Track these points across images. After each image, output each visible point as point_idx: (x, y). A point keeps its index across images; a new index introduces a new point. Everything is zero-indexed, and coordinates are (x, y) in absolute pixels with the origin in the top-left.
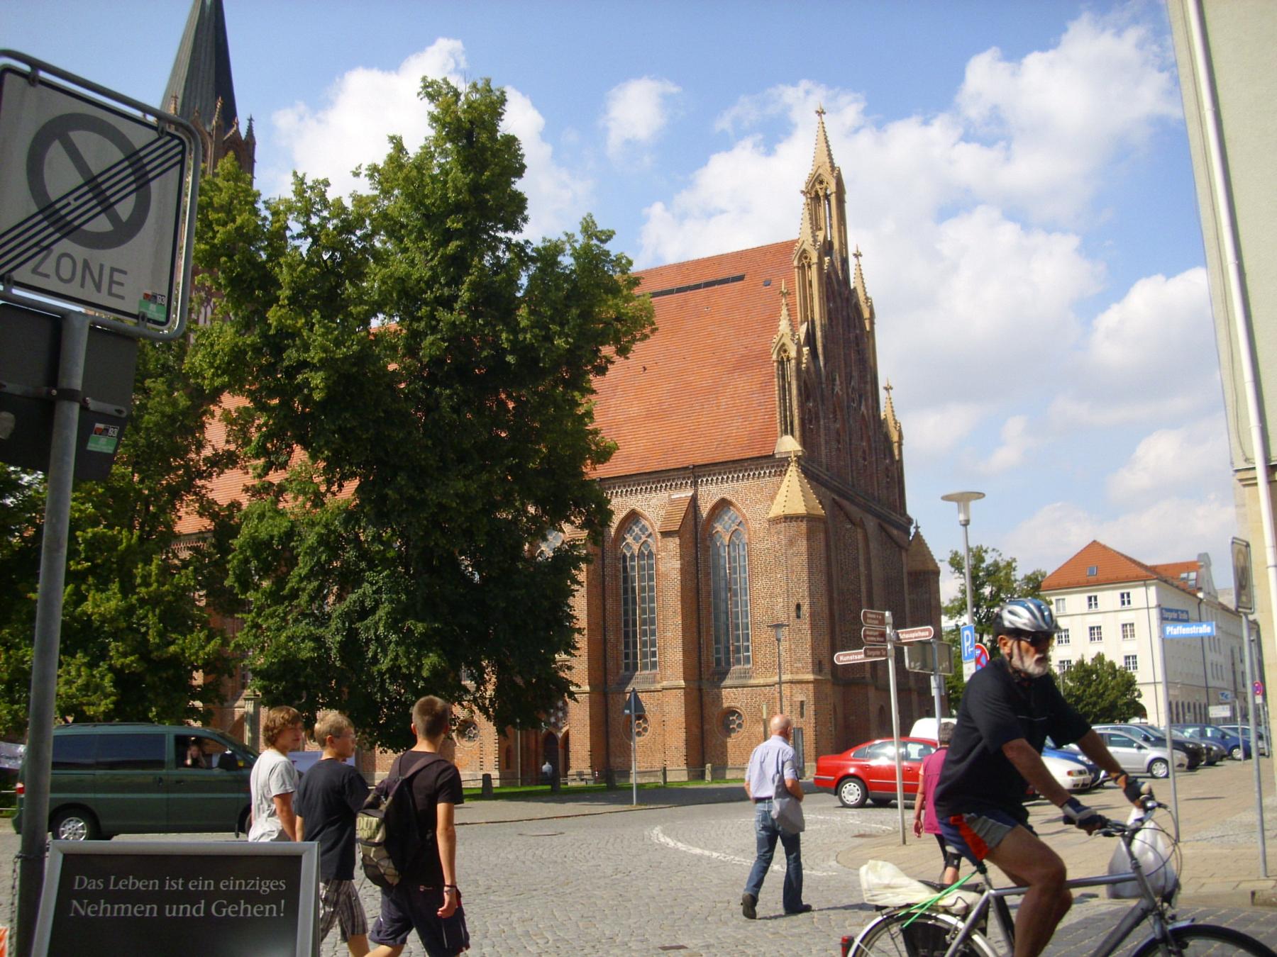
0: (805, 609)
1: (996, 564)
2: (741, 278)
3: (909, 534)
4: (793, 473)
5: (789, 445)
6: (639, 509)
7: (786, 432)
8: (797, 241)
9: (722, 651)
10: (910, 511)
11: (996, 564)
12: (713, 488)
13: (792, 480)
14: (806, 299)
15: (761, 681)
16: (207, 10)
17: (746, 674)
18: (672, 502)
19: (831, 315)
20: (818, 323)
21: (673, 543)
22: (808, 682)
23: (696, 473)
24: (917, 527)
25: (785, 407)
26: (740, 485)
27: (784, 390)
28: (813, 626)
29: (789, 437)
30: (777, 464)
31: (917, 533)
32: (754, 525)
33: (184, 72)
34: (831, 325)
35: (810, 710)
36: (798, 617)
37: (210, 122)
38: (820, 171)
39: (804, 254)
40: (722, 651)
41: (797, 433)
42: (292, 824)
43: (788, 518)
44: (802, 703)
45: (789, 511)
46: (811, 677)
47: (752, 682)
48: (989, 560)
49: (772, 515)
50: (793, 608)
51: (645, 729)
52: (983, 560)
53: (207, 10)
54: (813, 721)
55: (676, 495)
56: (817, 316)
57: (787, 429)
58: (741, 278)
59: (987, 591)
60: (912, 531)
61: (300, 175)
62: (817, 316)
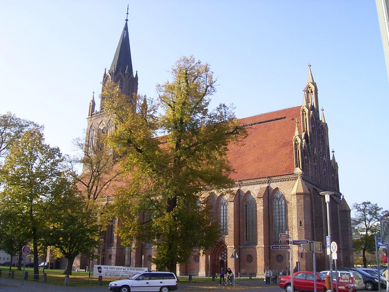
24: (343, 196)
29: (298, 168)
31: (343, 198)
41: (301, 167)
60: (342, 197)
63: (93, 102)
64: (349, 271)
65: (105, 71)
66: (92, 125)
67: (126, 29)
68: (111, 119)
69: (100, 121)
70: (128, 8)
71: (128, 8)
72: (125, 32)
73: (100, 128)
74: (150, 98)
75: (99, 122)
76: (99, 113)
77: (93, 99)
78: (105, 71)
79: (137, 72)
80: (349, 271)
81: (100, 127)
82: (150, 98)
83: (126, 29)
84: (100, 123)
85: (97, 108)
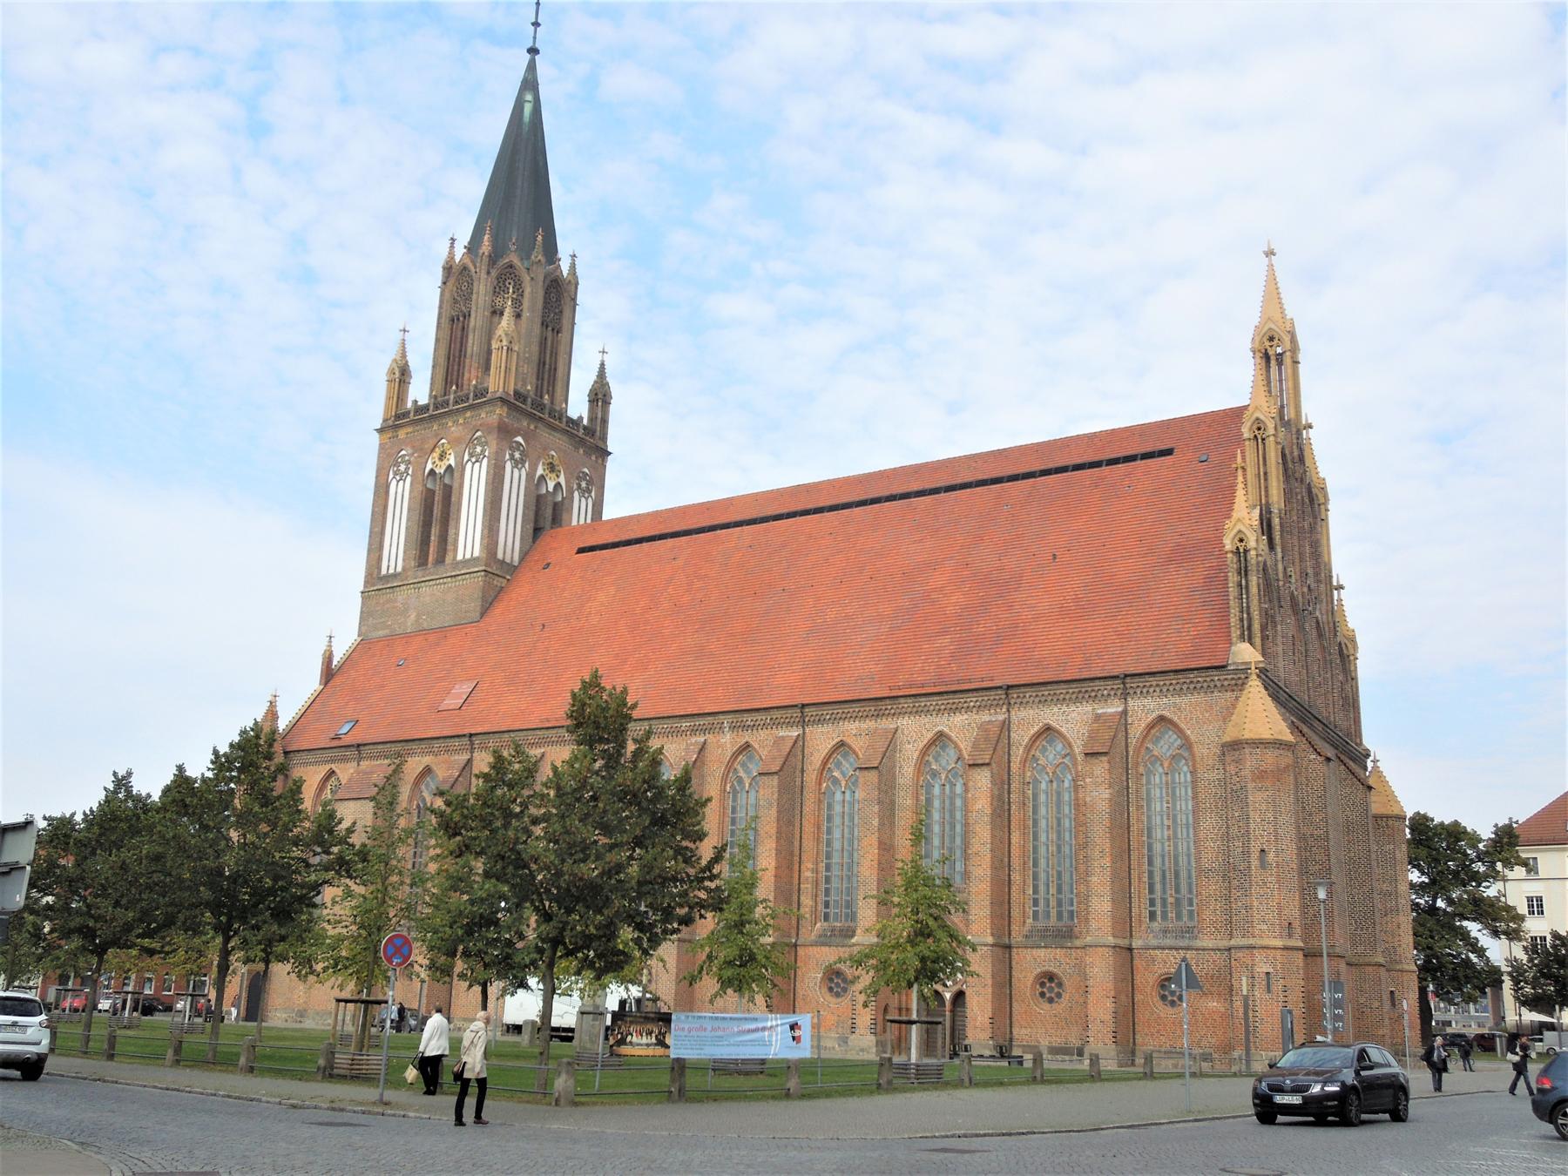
2: (1169, 452)
3: (1365, 769)
4: (1255, 687)
6: (1054, 725)
8: (1246, 408)
9: (1158, 902)
12: (1149, 703)
18: (1098, 717)
19: (1288, 494)
21: (1100, 768)
23: (1126, 682)
26: (1184, 701)
31: (1375, 768)
39: (1259, 426)
40: (1158, 902)
41: (1258, 641)
46: (1279, 943)
47: (1199, 943)
49: (1227, 738)
50: (1255, 855)
51: (1059, 995)
53: (526, 128)
55: (985, 717)
58: (1169, 452)
60: (1370, 765)
61: (121, 773)
64: (577, 406)
72: (529, 97)
73: (432, 471)
76: (425, 408)
77: (404, 355)
80: (577, 406)
81: (429, 466)
85: (420, 391)
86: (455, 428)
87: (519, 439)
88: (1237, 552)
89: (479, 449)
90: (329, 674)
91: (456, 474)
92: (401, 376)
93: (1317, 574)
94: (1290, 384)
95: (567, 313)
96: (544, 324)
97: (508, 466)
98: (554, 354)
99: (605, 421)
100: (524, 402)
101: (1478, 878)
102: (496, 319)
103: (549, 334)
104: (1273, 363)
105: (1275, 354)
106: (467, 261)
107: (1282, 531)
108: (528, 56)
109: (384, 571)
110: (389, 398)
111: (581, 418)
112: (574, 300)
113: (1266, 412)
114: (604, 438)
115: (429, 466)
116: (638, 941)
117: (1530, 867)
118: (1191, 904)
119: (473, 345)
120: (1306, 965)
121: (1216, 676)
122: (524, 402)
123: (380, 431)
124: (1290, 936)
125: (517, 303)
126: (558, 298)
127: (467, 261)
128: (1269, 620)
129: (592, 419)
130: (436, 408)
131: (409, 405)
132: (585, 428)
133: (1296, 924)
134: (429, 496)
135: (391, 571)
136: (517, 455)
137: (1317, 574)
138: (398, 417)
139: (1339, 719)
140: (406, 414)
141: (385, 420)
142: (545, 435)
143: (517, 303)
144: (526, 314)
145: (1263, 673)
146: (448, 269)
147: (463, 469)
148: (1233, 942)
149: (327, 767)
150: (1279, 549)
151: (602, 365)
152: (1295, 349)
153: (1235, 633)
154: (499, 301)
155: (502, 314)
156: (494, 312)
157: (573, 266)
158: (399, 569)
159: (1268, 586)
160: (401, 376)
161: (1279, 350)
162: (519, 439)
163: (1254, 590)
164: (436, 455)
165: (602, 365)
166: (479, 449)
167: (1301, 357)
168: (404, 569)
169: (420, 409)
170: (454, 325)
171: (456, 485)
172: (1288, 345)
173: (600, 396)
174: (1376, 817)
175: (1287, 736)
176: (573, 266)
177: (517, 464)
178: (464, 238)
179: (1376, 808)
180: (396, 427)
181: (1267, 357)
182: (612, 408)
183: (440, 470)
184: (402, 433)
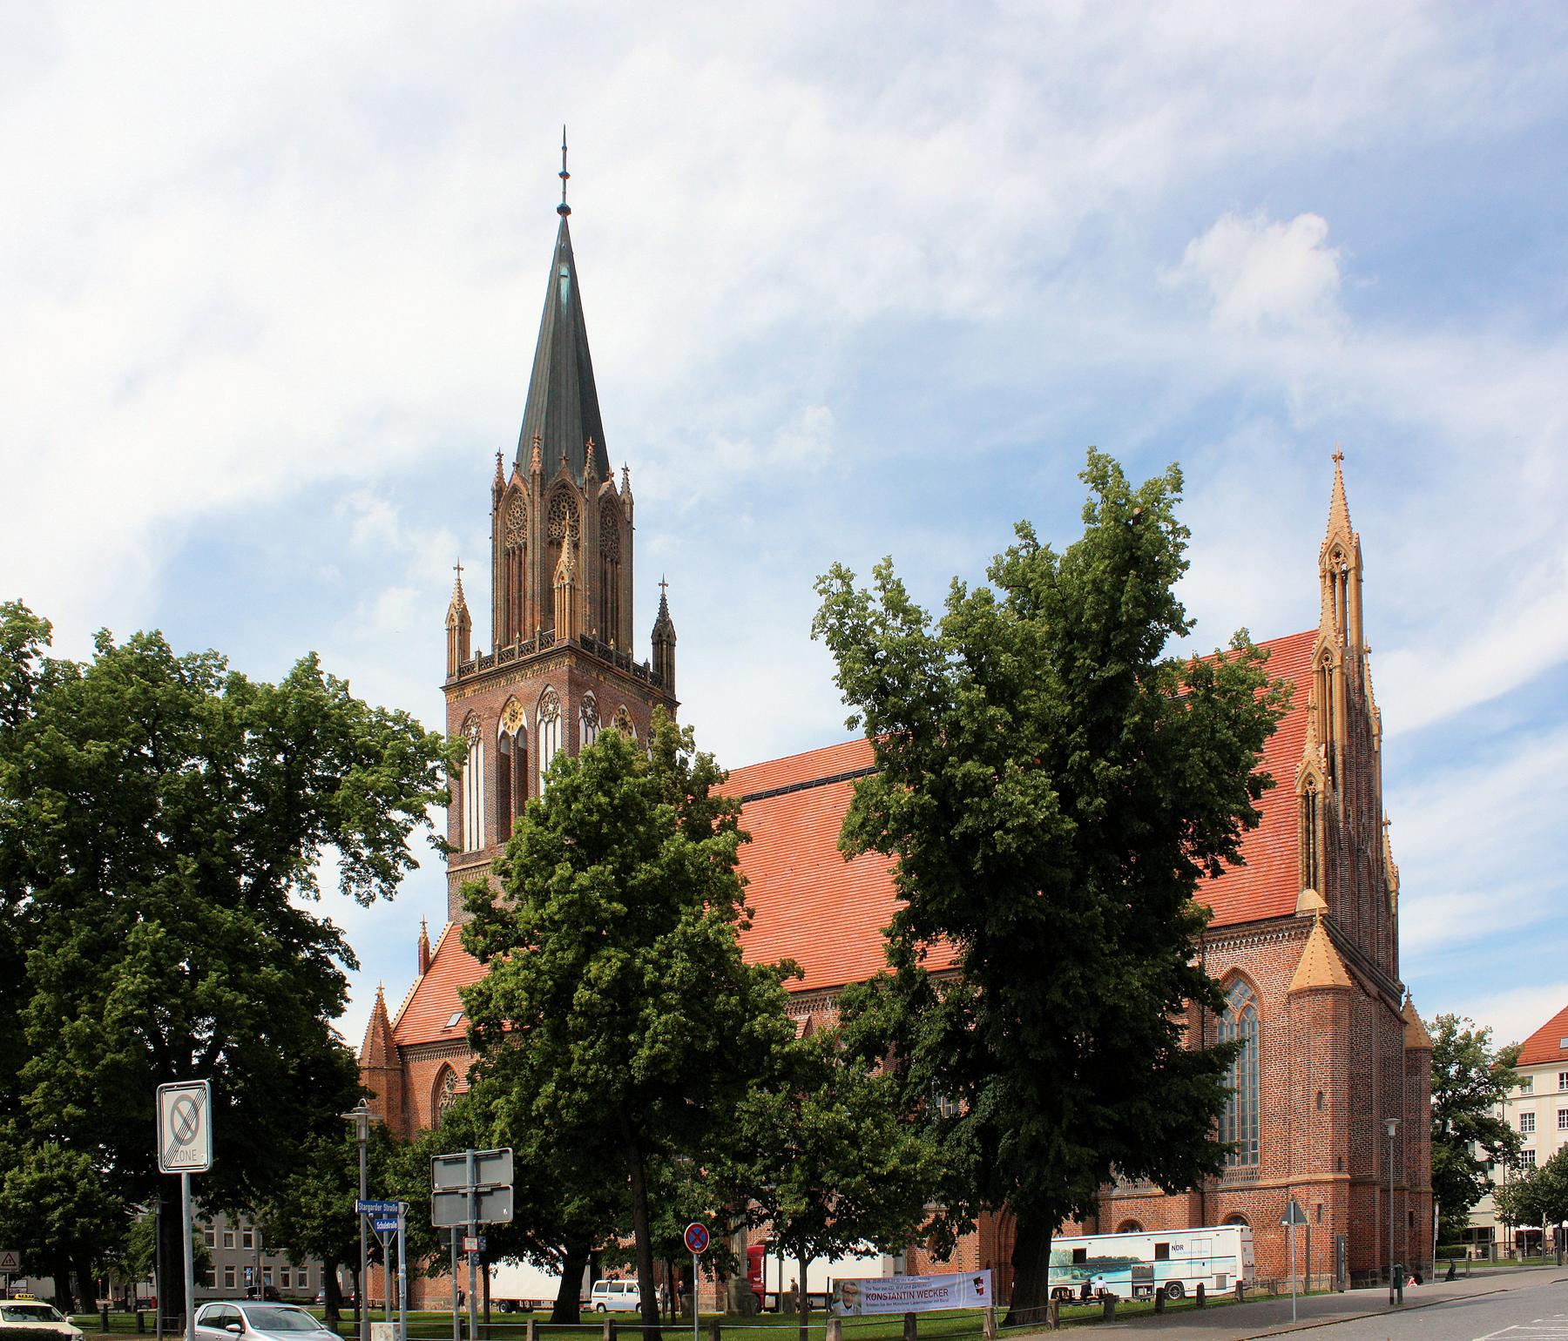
0: (1327, 1097)
1: (1467, 1036)
4: (1318, 935)
5: (1312, 901)
7: (1308, 885)
10: (1403, 977)
11: (1467, 1036)
13: (1318, 942)
14: (1327, 713)
15: (1271, 1182)
16: (564, 311)
17: (1253, 1175)
20: (1338, 745)
22: (1327, 1183)
24: (1408, 996)
25: (1310, 855)
27: (1309, 833)
28: (1334, 1118)
29: (1312, 891)
30: (1298, 926)
31: (1408, 1002)
32: (1268, 1000)
33: (543, 401)
34: (1350, 746)
35: (1327, 1214)
36: (1319, 1107)
37: (581, 474)
38: (1337, 540)
41: (1321, 886)
42: (1338, 1272)
43: (1315, 991)
44: (1320, 1206)
45: (1313, 983)
46: (1330, 1177)
47: (1261, 1183)
48: (1460, 1030)
49: (1293, 987)
50: (1314, 1097)
52: (1453, 1033)
53: (564, 311)
54: (1330, 1226)
56: (1337, 735)
57: (1311, 883)
59: (1453, 1070)
60: (1404, 1000)
62: (1337, 735)
63: (464, 618)
64: (643, 652)
65: (500, 464)
66: (466, 719)
67: (564, 254)
68: (550, 689)
69: (502, 700)
70: (565, 148)
71: (565, 148)
72: (564, 271)
73: (504, 733)
74: (626, 470)
75: (498, 705)
76: (490, 660)
77: (461, 598)
78: (500, 464)
79: (663, 584)
80: (643, 652)
81: (501, 728)
82: (626, 470)
83: (564, 254)
84: (503, 710)
85: (482, 641)
86: (526, 684)
87: (590, 693)
88: (1306, 797)
89: (551, 707)
90: (427, 964)
91: (531, 737)
92: (461, 626)
93: (1370, 810)
94: (1354, 604)
95: (623, 540)
96: (604, 556)
97: (582, 724)
98: (615, 590)
99: (671, 667)
100: (591, 650)
101: (1482, 1102)
102: (553, 551)
103: (609, 565)
104: (1338, 581)
105: (1024, 531)
106: (517, 481)
107: (1344, 769)
108: (559, 218)
109: (467, 849)
110: (451, 651)
111: (647, 664)
112: (630, 523)
113: (1331, 640)
114: (671, 686)
115: (501, 728)
116: (503, 1134)
117: (1525, 1083)
118: (1254, 1148)
119: (532, 583)
120: (1351, 1192)
121: (1284, 924)
122: (591, 650)
123: (446, 689)
124: (1340, 1170)
125: (574, 529)
126: (614, 519)
127: (517, 481)
128: (1331, 865)
129: (658, 664)
130: (501, 660)
131: (473, 657)
132: (652, 676)
133: (1345, 1158)
134: (503, 761)
135: (474, 848)
136: (589, 711)
137: (1370, 810)
138: (461, 672)
139: (1381, 956)
140: (470, 668)
141: (450, 676)
142: (610, 686)
143: (574, 529)
144: (584, 544)
145: (1329, 922)
146: (499, 491)
147: (537, 731)
148: (1291, 1179)
149: (442, 1061)
150: (1340, 789)
151: (663, 600)
152: (1359, 567)
153: (1301, 880)
154: (555, 532)
155: (560, 545)
156: (551, 543)
157: (626, 482)
158: (482, 846)
159: (1331, 829)
160: (461, 626)
161: (1344, 567)
162: (590, 693)
163: (1320, 834)
164: (507, 715)
165: (663, 600)
166: (551, 707)
167: (1365, 575)
168: (486, 845)
169: (485, 662)
170: (508, 560)
171: (531, 750)
172: (1352, 562)
173: (664, 638)
174: (1410, 1051)
175: (1348, 983)
176: (626, 482)
177: (591, 721)
178: (510, 457)
179: (1409, 1042)
180: (462, 685)
181: (1333, 576)
182: (677, 651)
183: (513, 733)
184: (469, 692)
